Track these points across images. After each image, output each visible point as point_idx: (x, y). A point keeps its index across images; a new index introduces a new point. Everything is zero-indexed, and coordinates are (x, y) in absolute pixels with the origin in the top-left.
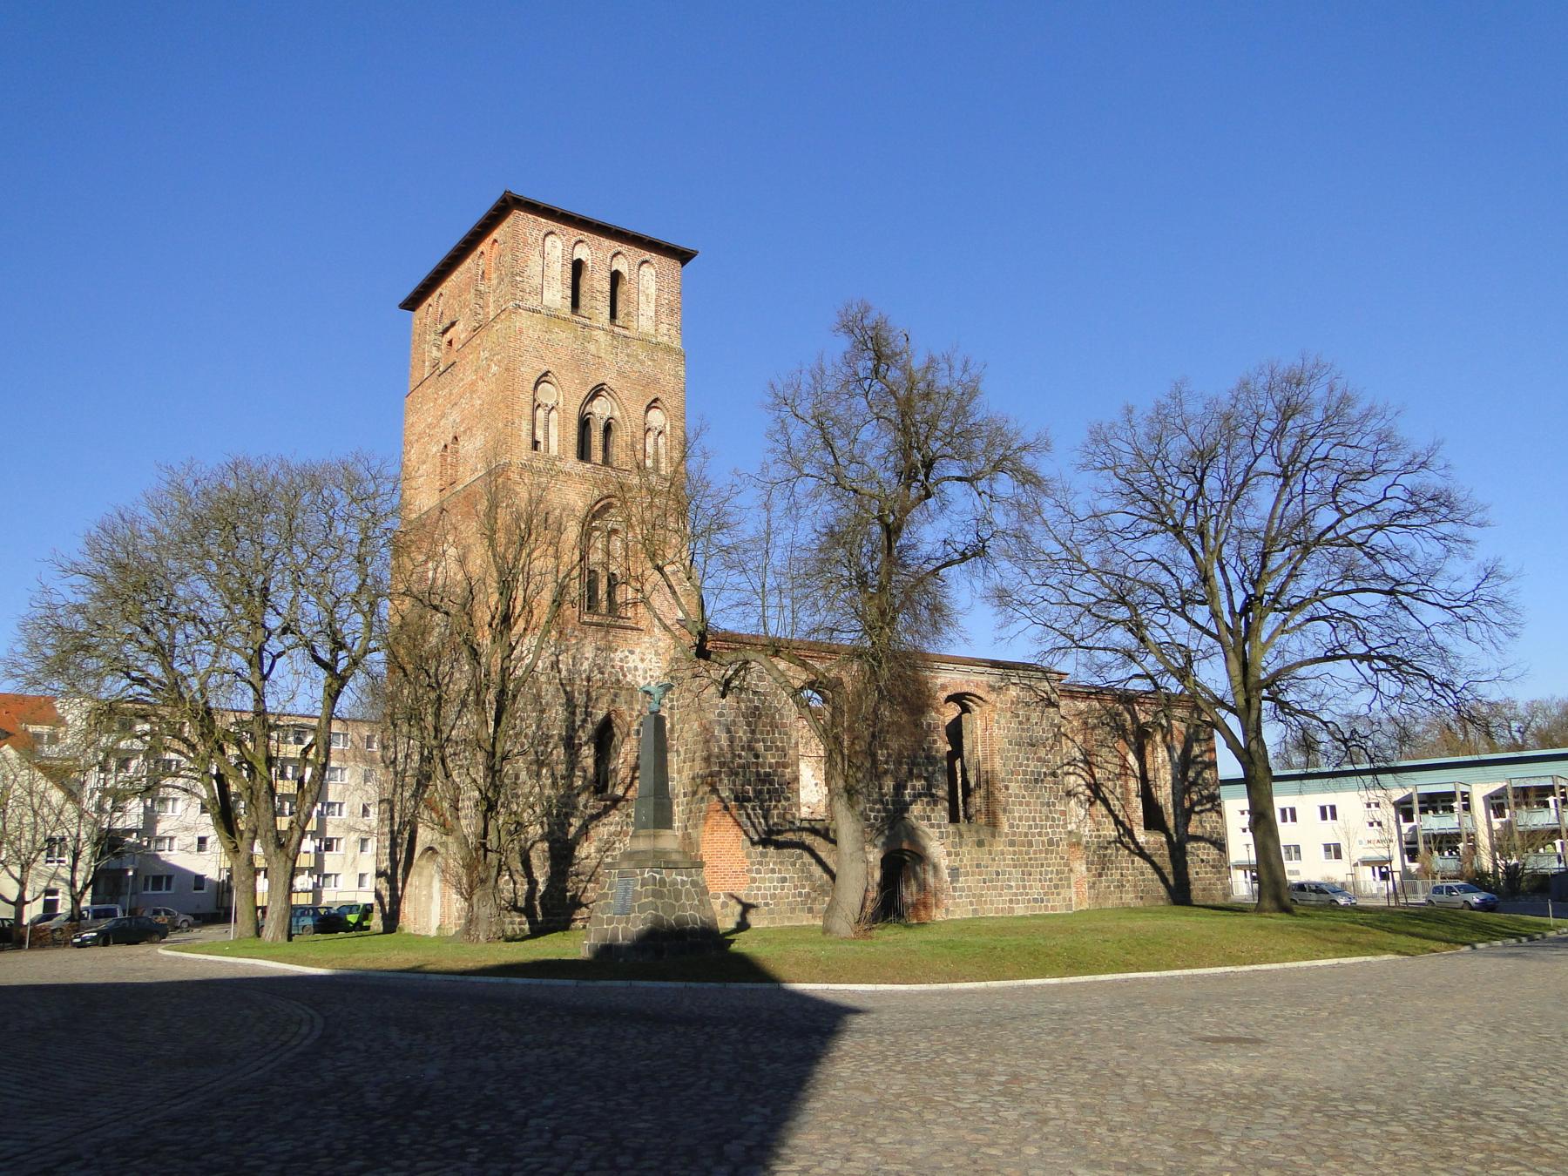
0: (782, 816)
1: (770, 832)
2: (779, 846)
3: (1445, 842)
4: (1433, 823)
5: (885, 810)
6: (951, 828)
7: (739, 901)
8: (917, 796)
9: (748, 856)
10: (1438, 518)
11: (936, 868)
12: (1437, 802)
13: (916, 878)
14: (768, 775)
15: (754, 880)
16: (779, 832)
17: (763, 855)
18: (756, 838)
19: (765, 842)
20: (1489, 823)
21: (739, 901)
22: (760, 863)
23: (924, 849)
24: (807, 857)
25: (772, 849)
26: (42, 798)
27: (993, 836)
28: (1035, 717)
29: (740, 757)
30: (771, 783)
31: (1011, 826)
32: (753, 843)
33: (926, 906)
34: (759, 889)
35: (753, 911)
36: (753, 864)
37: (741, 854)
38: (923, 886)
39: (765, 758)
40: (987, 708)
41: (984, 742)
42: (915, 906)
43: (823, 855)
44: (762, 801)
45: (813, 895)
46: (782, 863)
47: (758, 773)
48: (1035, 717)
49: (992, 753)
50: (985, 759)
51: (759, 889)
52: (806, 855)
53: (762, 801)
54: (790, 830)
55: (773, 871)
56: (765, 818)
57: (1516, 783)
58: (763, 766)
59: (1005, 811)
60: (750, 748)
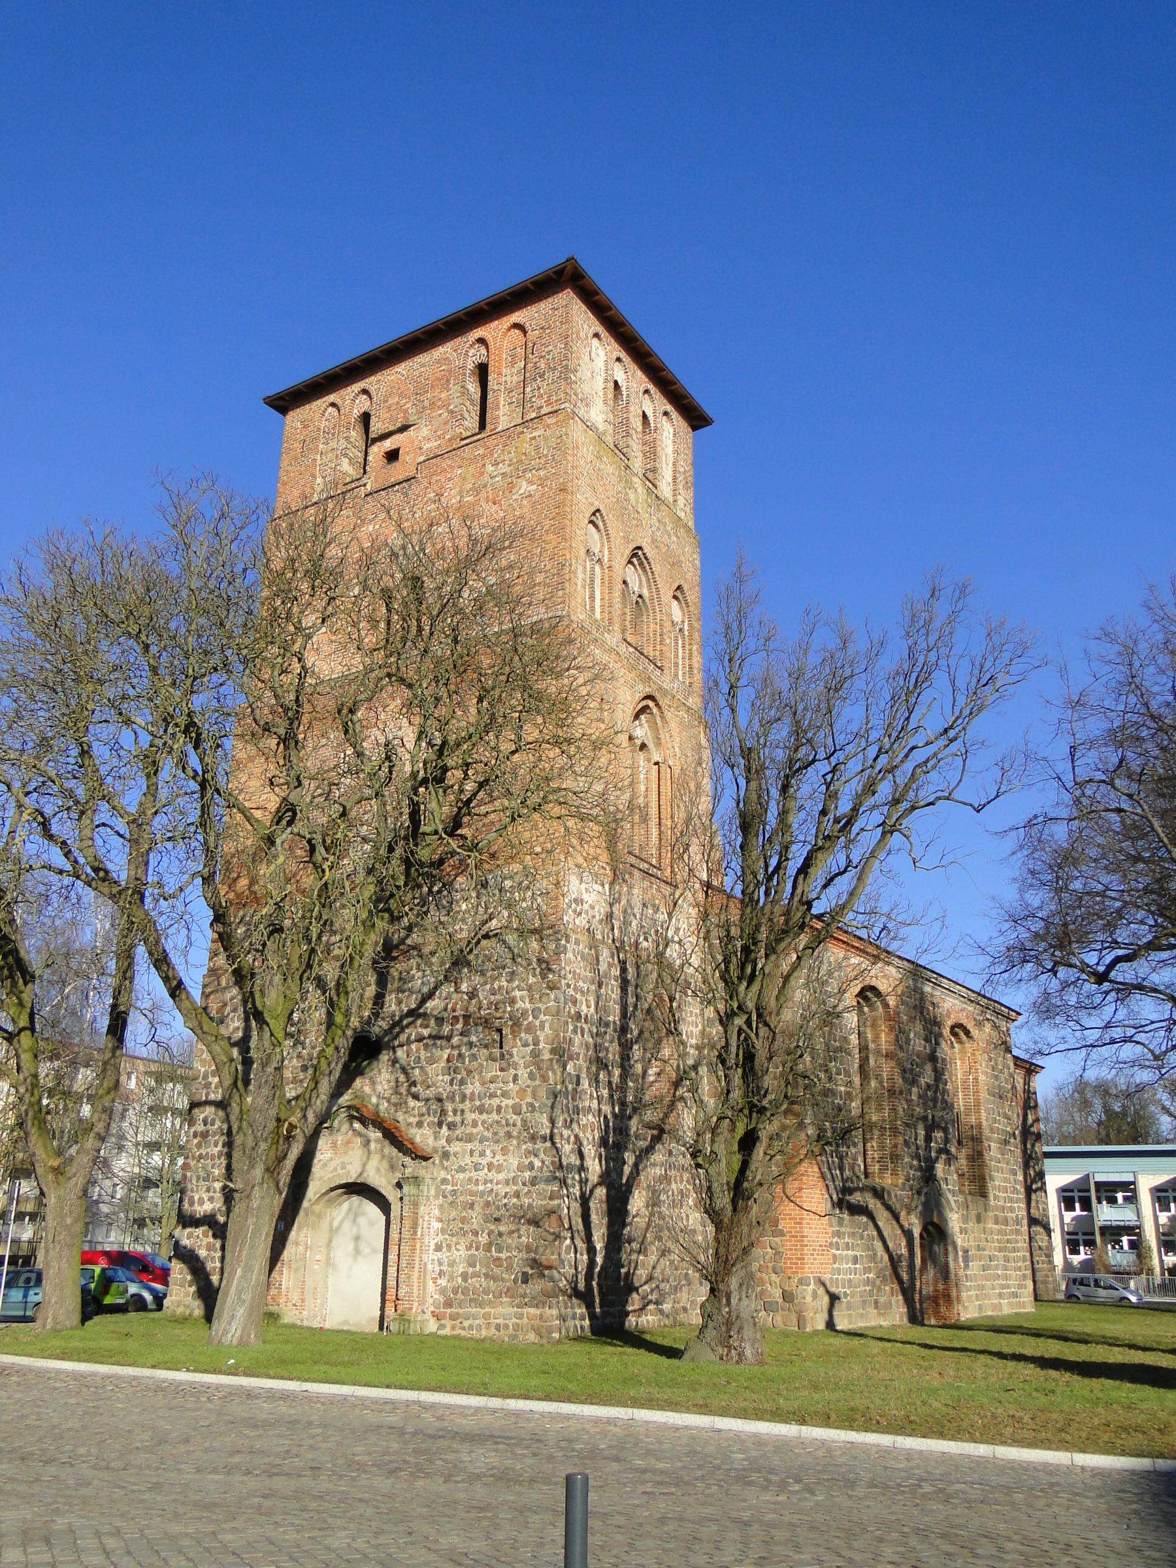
4: (1106, 1214)
12: (1108, 1191)
16: (850, 1191)
20: (1156, 1218)
31: (995, 1197)
33: (948, 1298)
38: (945, 1273)
42: (935, 1300)
49: (977, 1105)
57: (1100, 1178)
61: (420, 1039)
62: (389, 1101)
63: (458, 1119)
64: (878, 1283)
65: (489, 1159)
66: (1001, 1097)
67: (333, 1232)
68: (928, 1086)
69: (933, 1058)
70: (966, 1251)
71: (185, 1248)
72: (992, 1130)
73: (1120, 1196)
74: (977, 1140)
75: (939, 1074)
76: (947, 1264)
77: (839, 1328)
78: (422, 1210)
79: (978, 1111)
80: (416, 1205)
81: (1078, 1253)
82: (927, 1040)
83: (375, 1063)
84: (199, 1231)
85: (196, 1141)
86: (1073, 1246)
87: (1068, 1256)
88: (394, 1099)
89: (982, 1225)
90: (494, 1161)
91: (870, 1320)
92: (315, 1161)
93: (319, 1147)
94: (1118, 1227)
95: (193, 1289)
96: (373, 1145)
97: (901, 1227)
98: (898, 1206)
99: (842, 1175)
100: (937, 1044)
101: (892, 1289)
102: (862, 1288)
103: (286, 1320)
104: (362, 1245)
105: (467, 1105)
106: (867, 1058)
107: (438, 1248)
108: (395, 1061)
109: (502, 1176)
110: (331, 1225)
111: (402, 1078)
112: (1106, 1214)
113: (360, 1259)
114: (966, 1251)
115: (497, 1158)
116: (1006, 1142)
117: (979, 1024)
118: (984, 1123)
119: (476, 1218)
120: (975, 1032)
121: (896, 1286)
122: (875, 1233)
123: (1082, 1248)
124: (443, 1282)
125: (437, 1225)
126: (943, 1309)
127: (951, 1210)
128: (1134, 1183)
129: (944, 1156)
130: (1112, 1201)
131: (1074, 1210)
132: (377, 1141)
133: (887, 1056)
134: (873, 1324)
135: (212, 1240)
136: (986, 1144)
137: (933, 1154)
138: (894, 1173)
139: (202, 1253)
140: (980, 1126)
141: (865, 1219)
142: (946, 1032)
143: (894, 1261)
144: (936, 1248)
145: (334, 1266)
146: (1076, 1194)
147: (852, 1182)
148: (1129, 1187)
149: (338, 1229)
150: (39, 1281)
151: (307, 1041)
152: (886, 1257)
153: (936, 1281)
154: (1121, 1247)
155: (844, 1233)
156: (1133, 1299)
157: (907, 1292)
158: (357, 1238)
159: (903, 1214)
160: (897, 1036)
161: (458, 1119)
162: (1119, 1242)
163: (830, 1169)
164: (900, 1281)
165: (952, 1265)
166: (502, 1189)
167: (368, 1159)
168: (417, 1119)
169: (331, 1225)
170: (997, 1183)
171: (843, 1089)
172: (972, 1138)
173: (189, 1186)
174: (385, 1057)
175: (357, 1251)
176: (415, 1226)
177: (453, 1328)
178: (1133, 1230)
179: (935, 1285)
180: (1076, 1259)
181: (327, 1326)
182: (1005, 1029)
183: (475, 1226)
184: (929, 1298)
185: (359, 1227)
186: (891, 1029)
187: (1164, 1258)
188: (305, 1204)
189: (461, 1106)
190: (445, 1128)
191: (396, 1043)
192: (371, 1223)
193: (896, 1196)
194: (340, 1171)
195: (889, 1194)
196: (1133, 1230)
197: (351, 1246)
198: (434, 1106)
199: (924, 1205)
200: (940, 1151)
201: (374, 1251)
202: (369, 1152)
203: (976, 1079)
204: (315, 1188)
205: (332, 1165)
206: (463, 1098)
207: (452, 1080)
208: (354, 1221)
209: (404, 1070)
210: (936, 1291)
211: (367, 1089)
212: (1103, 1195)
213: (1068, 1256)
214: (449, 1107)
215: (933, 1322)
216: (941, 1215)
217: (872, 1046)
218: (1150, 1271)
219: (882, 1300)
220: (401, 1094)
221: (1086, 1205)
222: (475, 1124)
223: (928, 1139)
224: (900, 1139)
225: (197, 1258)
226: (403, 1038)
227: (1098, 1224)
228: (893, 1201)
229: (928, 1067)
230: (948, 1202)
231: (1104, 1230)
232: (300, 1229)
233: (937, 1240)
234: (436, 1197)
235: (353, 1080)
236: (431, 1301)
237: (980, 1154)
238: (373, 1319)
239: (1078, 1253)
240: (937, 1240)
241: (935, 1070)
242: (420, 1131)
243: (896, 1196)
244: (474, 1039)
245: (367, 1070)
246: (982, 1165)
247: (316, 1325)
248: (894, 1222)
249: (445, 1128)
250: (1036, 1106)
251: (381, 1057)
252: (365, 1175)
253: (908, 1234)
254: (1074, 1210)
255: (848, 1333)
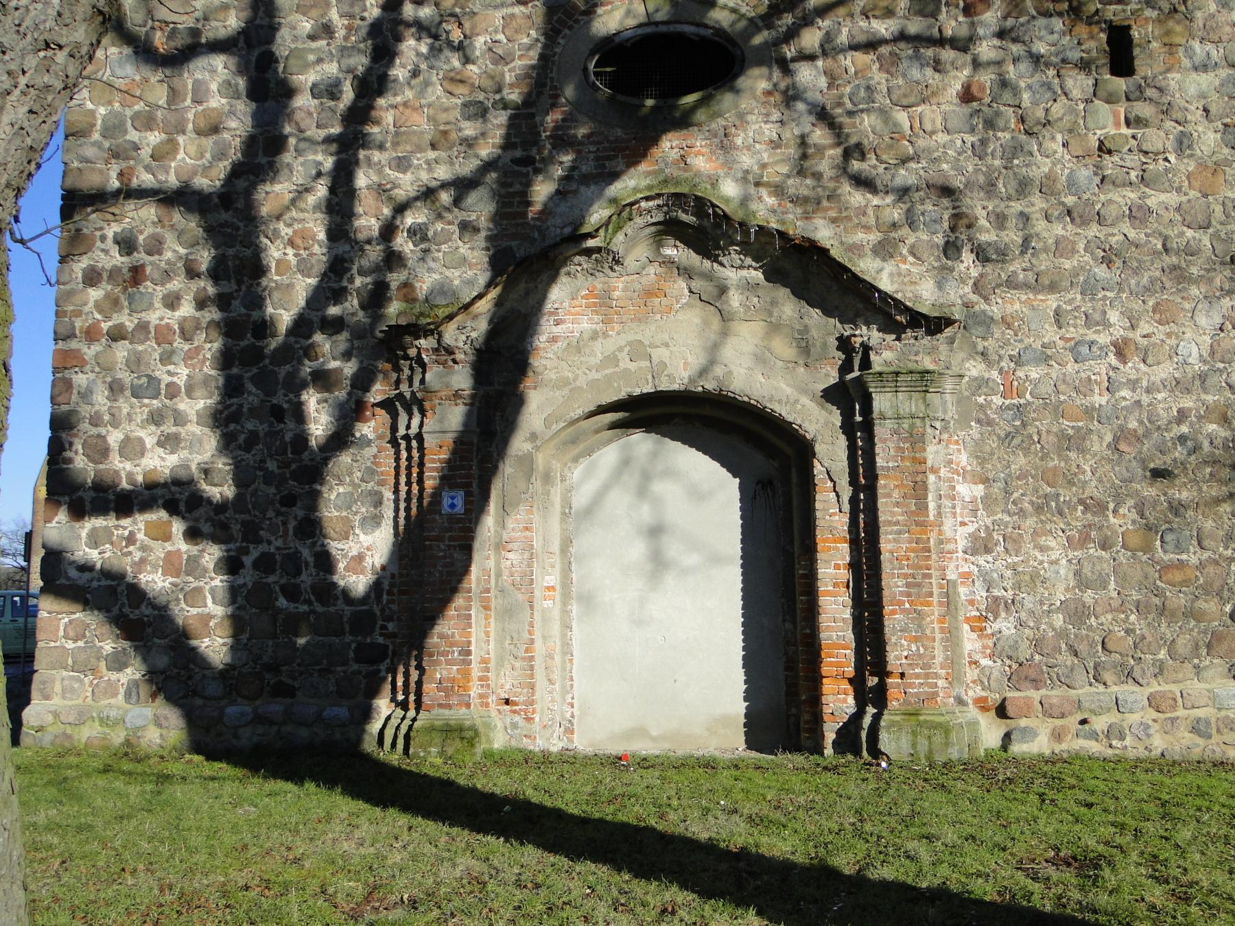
61: (871, 45)
62: (778, 190)
63: (1012, 236)
65: (1118, 333)
67: (578, 518)
71: (86, 568)
78: (933, 453)
80: (916, 441)
83: (727, 99)
84: (139, 524)
85: (95, 294)
88: (803, 187)
90: (1136, 336)
92: (541, 340)
93: (548, 306)
95: (133, 672)
96: (735, 299)
103: (499, 741)
104: (673, 548)
105: (1037, 203)
107: (981, 545)
108: (790, 97)
109: (1164, 371)
110: (567, 504)
111: (819, 135)
113: (670, 579)
115: (1145, 327)
119: (1092, 470)
124: (1005, 625)
125: (968, 491)
132: (750, 287)
135: (183, 546)
139: (155, 581)
145: (587, 600)
149: (589, 511)
150: (477, 733)
151: (480, 42)
158: (655, 531)
161: (1012, 236)
166: (1165, 404)
167: (725, 333)
168: (874, 237)
169: (567, 504)
173: (85, 410)
174: (757, 81)
175: (658, 563)
176: (919, 490)
177: (1057, 736)
181: (582, 743)
183: (1093, 490)
185: (657, 503)
188: (519, 444)
189: (1017, 206)
190: (968, 257)
191: (789, 52)
192: (697, 495)
194: (625, 363)
197: (637, 550)
198: (932, 209)
201: (716, 559)
202: (725, 317)
204: (542, 407)
205: (600, 349)
206: (1023, 187)
207: (984, 142)
208: (642, 491)
209: (823, 115)
211: (701, 163)
214: (979, 208)
220: (818, 176)
222: (1062, 248)
225: (136, 594)
226: (811, 39)
232: (504, 509)
234: (963, 422)
235: (654, 141)
236: (971, 674)
238: (725, 721)
242: (889, 267)
244: (1041, 48)
245: (700, 115)
247: (555, 746)
249: (968, 257)
251: (742, 82)
252: (719, 371)
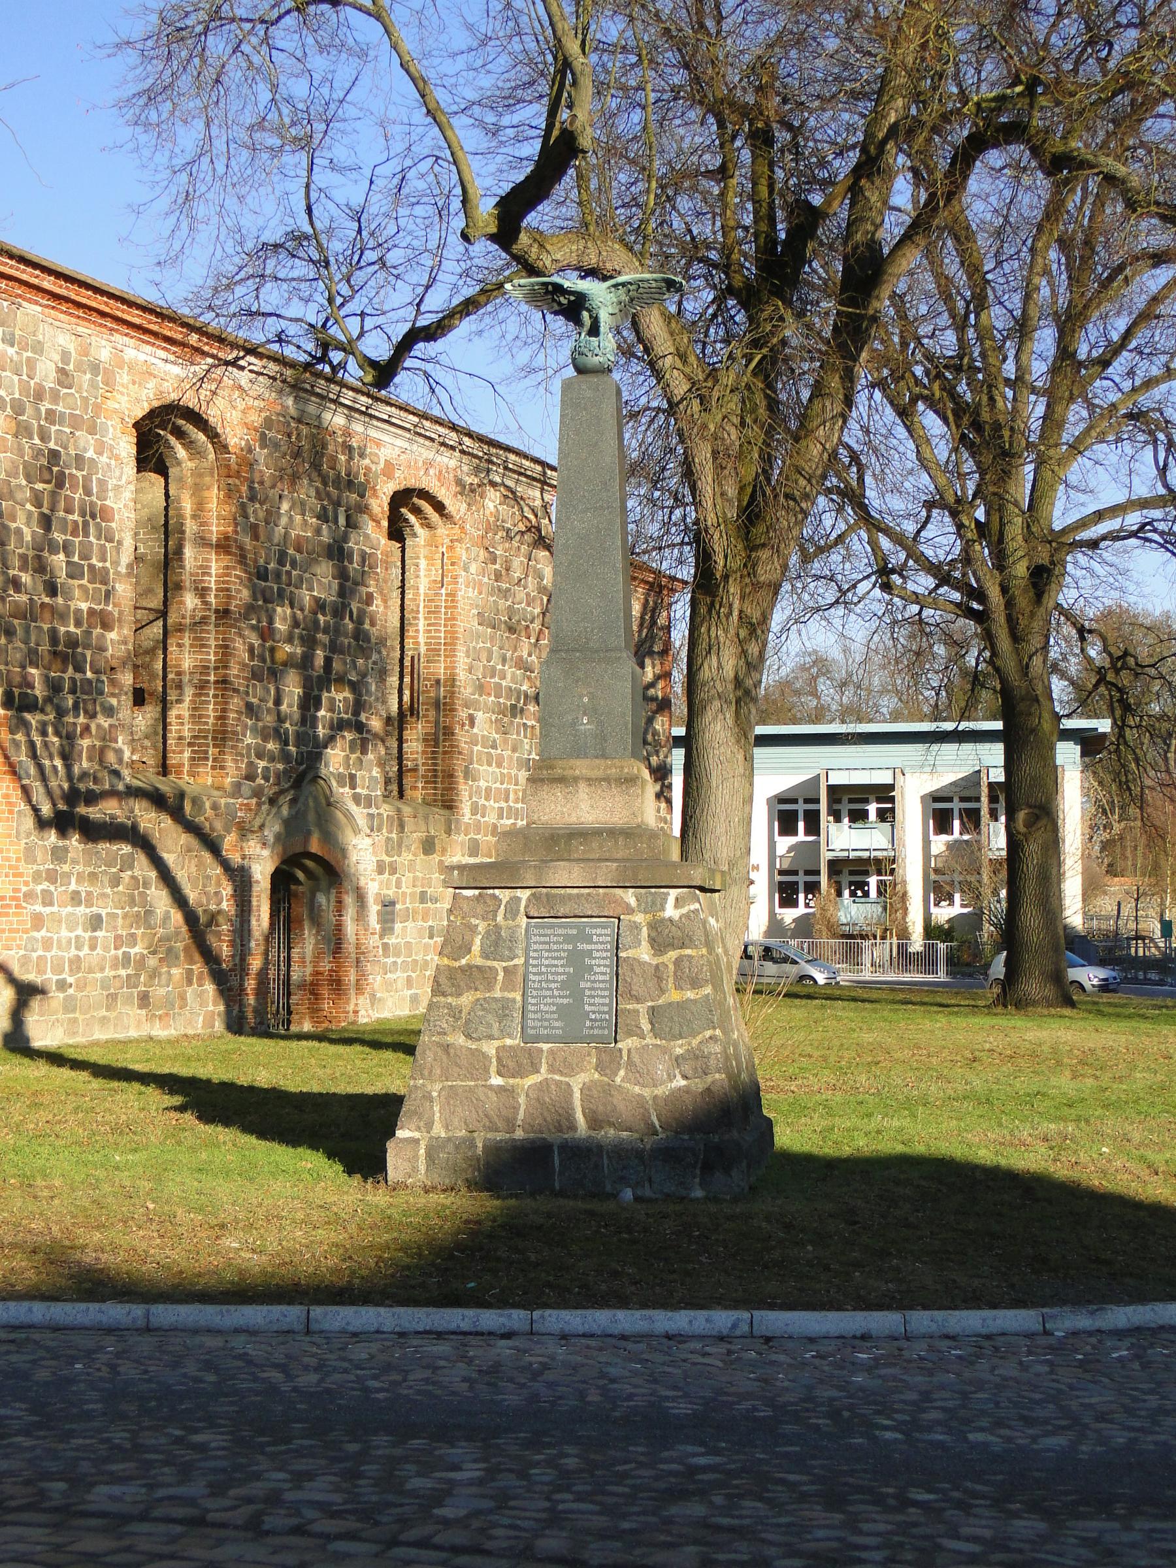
0: (99, 754)
1: (73, 796)
2: (93, 832)
3: (853, 872)
4: (843, 839)
5: (285, 757)
6: (386, 810)
7: (12, 980)
8: (339, 726)
9: (29, 855)
10: (302, 254)
11: (361, 898)
12: (853, 802)
13: (316, 920)
14: (73, 642)
15: (38, 921)
16: (92, 798)
17: (58, 855)
18: (46, 809)
19: (63, 822)
20: (927, 843)
21: (12, 980)
22: (52, 877)
23: (344, 852)
24: (143, 868)
25: (74, 841)
26: (1012, 429)
27: (449, 832)
28: (518, 563)
29: (16, 584)
30: (79, 669)
31: (475, 810)
32: (42, 824)
33: (337, 985)
34: (47, 944)
35: (35, 1003)
36: (37, 877)
37: (15, 851)
38: (335, 943)
39: (68, 597)
40: (443, 530)
41: (432, 612)
42: (312, 989)
43: (169, 858)
44: (61, 713)
45: (152, 962)
46: (93, 876)
47: (53, 634)
48: (518, 563)
49: (451, 643)
50: (433, 651)
51: (47, 944)
52: (141, 859)
53: (61, 713)
54: (113, 793)
55: (75, 898)
56: (66, 757)
57: (837, 779)
58: (63, 617)
59: (467, 774)
60: (41, 567)
64: (152, 962)
66: (512, 630)
68: (320, 605)
69: (337, 552)
70: (388, 905)
72: (481, 688)
73: (872, 808)
74: (444, 706)
75: (349, 584)
76: (339, 927)
77: (37, 1043)
79: (451, 654)
81: (794, 904)
82: (323, 517)
86: (786, 894)
87: (778, 910)
89: (436, 858)
91: (123, 1030)
94: (860, 860)
97: (225, 865)
98: (218, 825)
99: (68, 767)
100: (351, 524)
101: (189, 973)
102: (109, 973)
106: (179, 551)
112: (843, 839)
114: (388, 905)
116: (515, 711)
117: (468, 492)
118: (462, 676)
120: (454, 505)
121: (198, 967)
122: (153, 874)
123: (801, 896)
126: (326, 1005)
127: (357, 831)
128: (891, 787)
129: (349, 736)
130: (859, 816)
131: (794, 832)
133: (218, 546)
134: (133, 1033)
136: (463, 714)
137: (321, 731)
138: (219, 765)
140: (452, 680)
141: (126, 849)
142: (380, 504)
143: (197, 927)
144: (321, 899)
146: (801, 807)
147: (96, 780)
148: (884, 793)
152: (177, 917)
153: (317, 957)
154: (866, 894)
155: (68, 875)
156: (821, 978)
157: (227, 982)
159: (229, 842)
160: (243, 507)
162: (862, 885)
163: (34, 756)
164: (209, 956)
165: (350, 928)
170: (483, 784)
171: (84, 606)
172: (437, 704)
178: (883, 865)
179: (315, 963)
180: (789, 915)
182: (538, 503)
184: (302, 986)
186: (230, 492)
187: (933, 910)
193: (215, 807)
195: (196, 801)
196: (883, 865)
199: (287, 823)
200: (339, 726)
203: (452, 595)
210: (317, 973)
212: (845, 807)
213: (778, 910)
215: (307, 1027)
216: (329, 837)
217: (190, 527)
218: (904, 934)
219: (159, 992)
221: (813, 827)
223: (310, 702)
224: (236, 703)
227: (825, 856)
228: (206, 817)
229: (325, 570)
230: (349, 816)
231: (835, 866)
233: (324, 884)
237: (449, 732)
239: (794, 904)
240: (324, 884)
241: (342, 575)
243: (215, 807)
246: (452, 751)
248: (207, 856)
250: (665, 652)
253: (240, 879)
254: (794, 832)
255: (56, 1058)
